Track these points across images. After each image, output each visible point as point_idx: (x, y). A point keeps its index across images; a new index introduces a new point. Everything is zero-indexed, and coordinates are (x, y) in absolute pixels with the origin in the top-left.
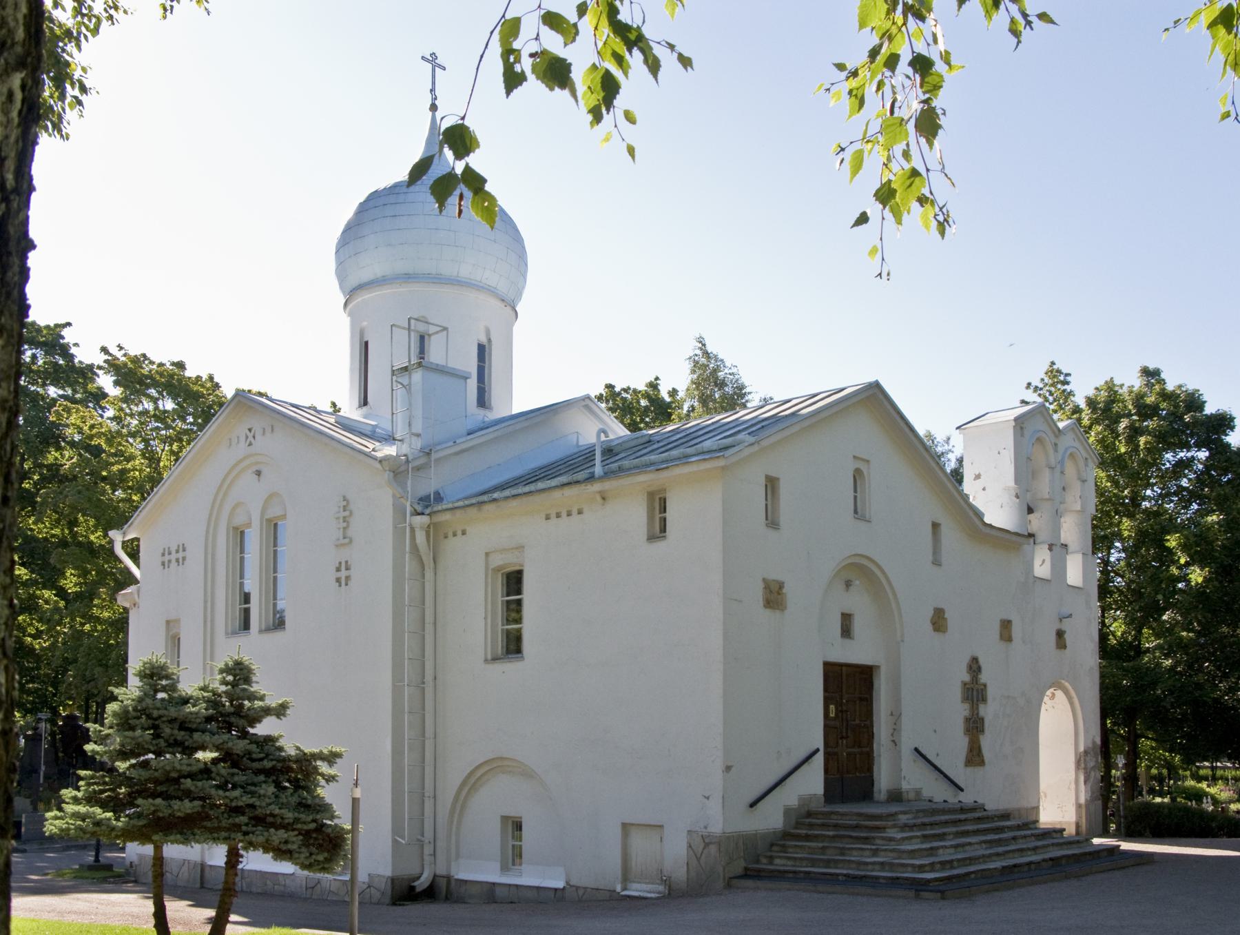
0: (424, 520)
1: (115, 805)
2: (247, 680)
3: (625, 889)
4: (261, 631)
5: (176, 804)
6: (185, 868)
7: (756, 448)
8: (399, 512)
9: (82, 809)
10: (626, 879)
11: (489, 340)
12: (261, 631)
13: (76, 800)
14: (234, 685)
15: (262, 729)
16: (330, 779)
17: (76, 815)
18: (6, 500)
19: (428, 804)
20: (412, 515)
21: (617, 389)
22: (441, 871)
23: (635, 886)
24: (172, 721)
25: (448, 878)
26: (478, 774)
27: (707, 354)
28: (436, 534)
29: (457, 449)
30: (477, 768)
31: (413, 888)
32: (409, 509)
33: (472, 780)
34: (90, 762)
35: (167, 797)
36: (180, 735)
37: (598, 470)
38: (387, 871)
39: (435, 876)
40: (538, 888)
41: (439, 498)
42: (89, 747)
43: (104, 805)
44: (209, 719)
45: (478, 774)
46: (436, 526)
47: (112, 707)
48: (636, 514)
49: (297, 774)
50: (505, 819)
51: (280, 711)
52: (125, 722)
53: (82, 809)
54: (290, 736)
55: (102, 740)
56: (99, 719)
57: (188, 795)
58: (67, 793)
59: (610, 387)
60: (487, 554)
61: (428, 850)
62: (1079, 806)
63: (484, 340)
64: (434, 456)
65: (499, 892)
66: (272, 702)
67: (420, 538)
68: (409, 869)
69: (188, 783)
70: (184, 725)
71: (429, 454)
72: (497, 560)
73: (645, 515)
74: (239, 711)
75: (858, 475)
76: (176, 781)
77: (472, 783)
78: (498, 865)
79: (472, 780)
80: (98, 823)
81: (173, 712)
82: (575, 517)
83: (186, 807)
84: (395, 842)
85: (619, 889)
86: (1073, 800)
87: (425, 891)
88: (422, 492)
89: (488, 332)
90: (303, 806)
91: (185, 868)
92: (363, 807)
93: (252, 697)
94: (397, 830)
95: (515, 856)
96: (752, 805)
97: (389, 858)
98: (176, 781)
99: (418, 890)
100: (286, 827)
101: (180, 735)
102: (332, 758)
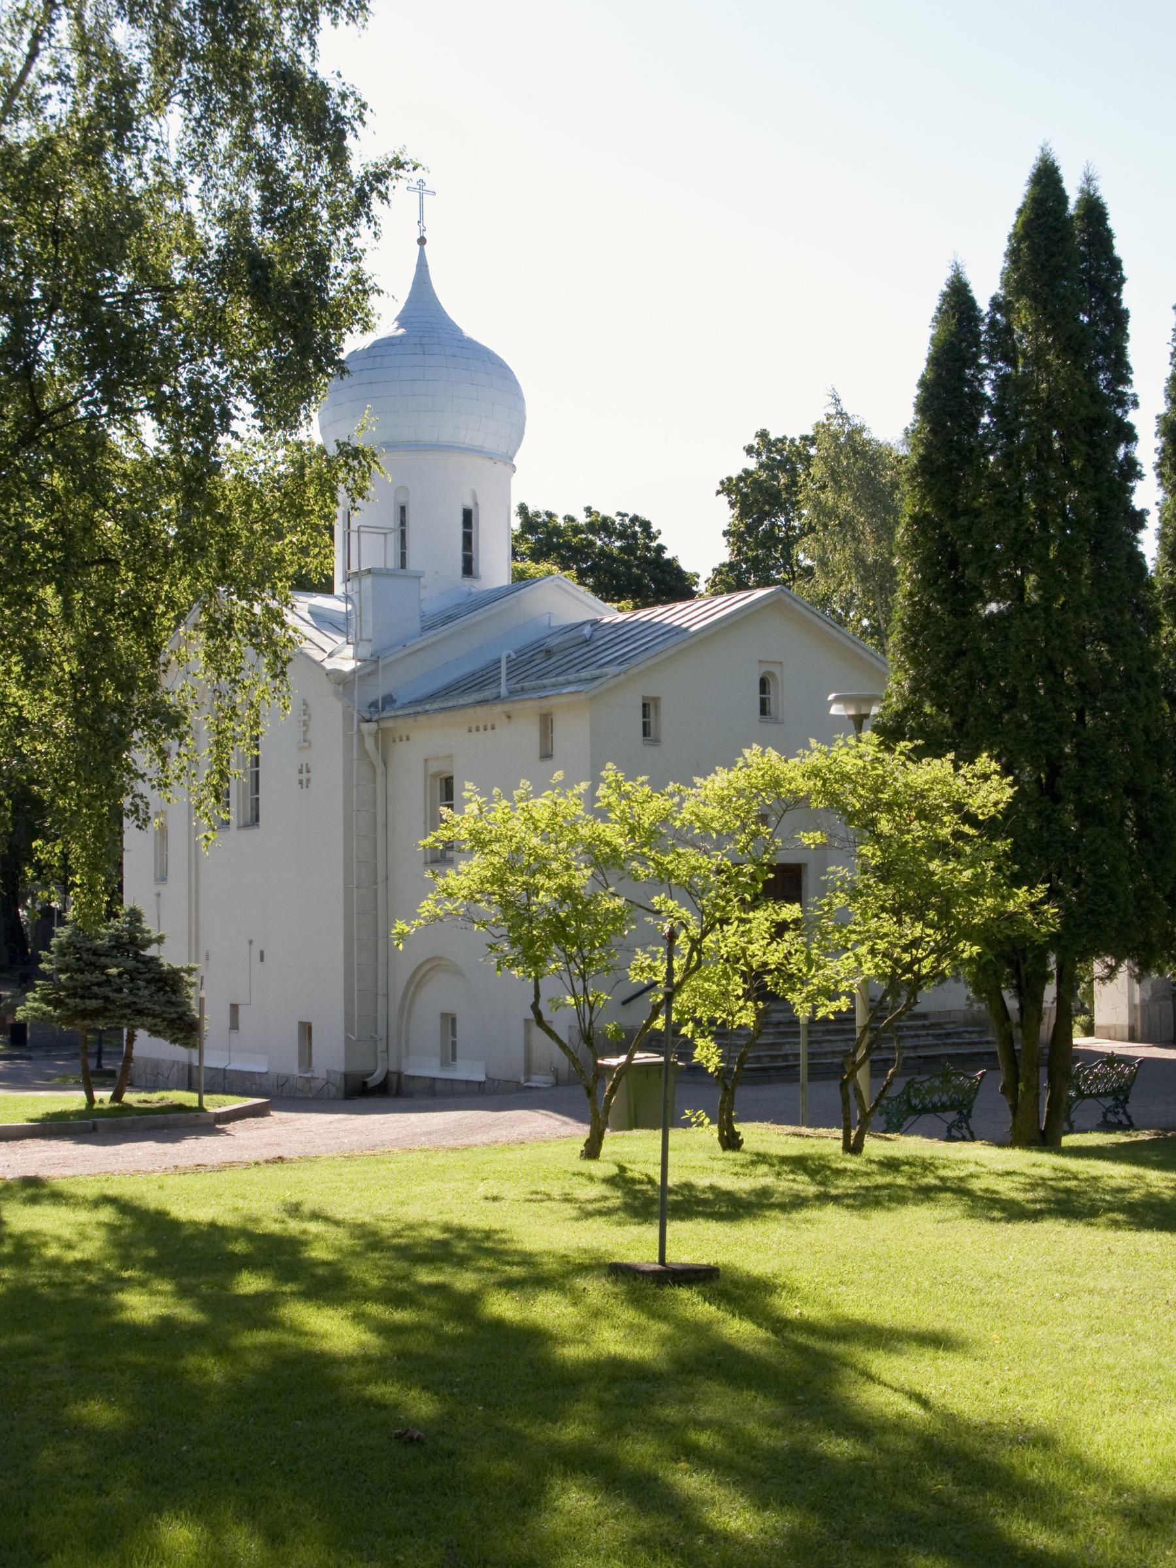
0: (372, 726)
1: (57, 1003)
2: (139, 920)
3: (528, 1080)
4: (239, 827)
5: (88, 1002)
6: (175, 1070)
7: (622, 677)
8: (347, 717)
9: (36, 1005)
10: (528, 1071)
11: (476, 504)
12: (239, 827)
13: (35, 1000)
14: (131, 923)
15: (151, 952)
16: (193, 985)
17: (32, 1009)
18: (8, 108)
19: (381, 1001)
20: (359, 722)
21: (772, 437)
22: (393, 1068)
23: (535, 1077)
24: (89, 950)
25: (399, 1074)
26: (422, 972)
27: (841, 414)
28: (384, 739)
29: (407, 651)
30: (422, 965)
31: (365, 1083)
32: (356, 716)
33: (418, 977)
34: (44, 976)
35: (82, 997)
36: (93, 959)
37: (503, 691)
38: (340, 1067)
39: (388, 1072)
40: (467, 1082)
41: (389, 700)
42: (42, 966)
43: (48, 1003)
44: (113, 947)
45: (422, 972)
46: (384, 731)
47: (54, 941)
48: (530, 733)
49: (169, 983)
50: (444, 1016)
51: (160, 940)
52: (62, 950)
53: (36, 1005)
54: (170, 956)
55: (50, 962)
56: (47, 948)
57: (96, 996)
58: (30, 995)
59: (763, 435)
60: (426, 761)
61: (381, 1046)
62: (1132, 1007)
63: (469, 504)
64: (381, 663)
65: (439, 1086)
66: (154, 935)
67: (369, 743)
68: (362, 1065)
69: (95, 989)
70: (95, 952)
71: (377, 662)
72: (434, 767)
73: (537, 734)
74: (133, 940)
75: (764, 684)
76: (89, 988)
77: (418, 980)
78: (438, 1061)
79: (418, 977)
80: (44, 1013)
81: (88, 945)
82: (489, 731)
83: (93, 1004)
84: (347, 1039)
85: (522, 1080)
86: (1126, 1000)
87: (379, 1086)
88: (371, 698)
89: (474, 495)
90: (170, 1003)
91: (175, 1070)
92: (206, 1003)
93: (142, 931)
94: (348, 1028)
95: (450, 1055)
96: (624, 1003)
97: (342, 1054)
98: (89, 988)
99: (371, 1085)
100: (154, 1016)
101: (93, 959)
102: (190, 971)
